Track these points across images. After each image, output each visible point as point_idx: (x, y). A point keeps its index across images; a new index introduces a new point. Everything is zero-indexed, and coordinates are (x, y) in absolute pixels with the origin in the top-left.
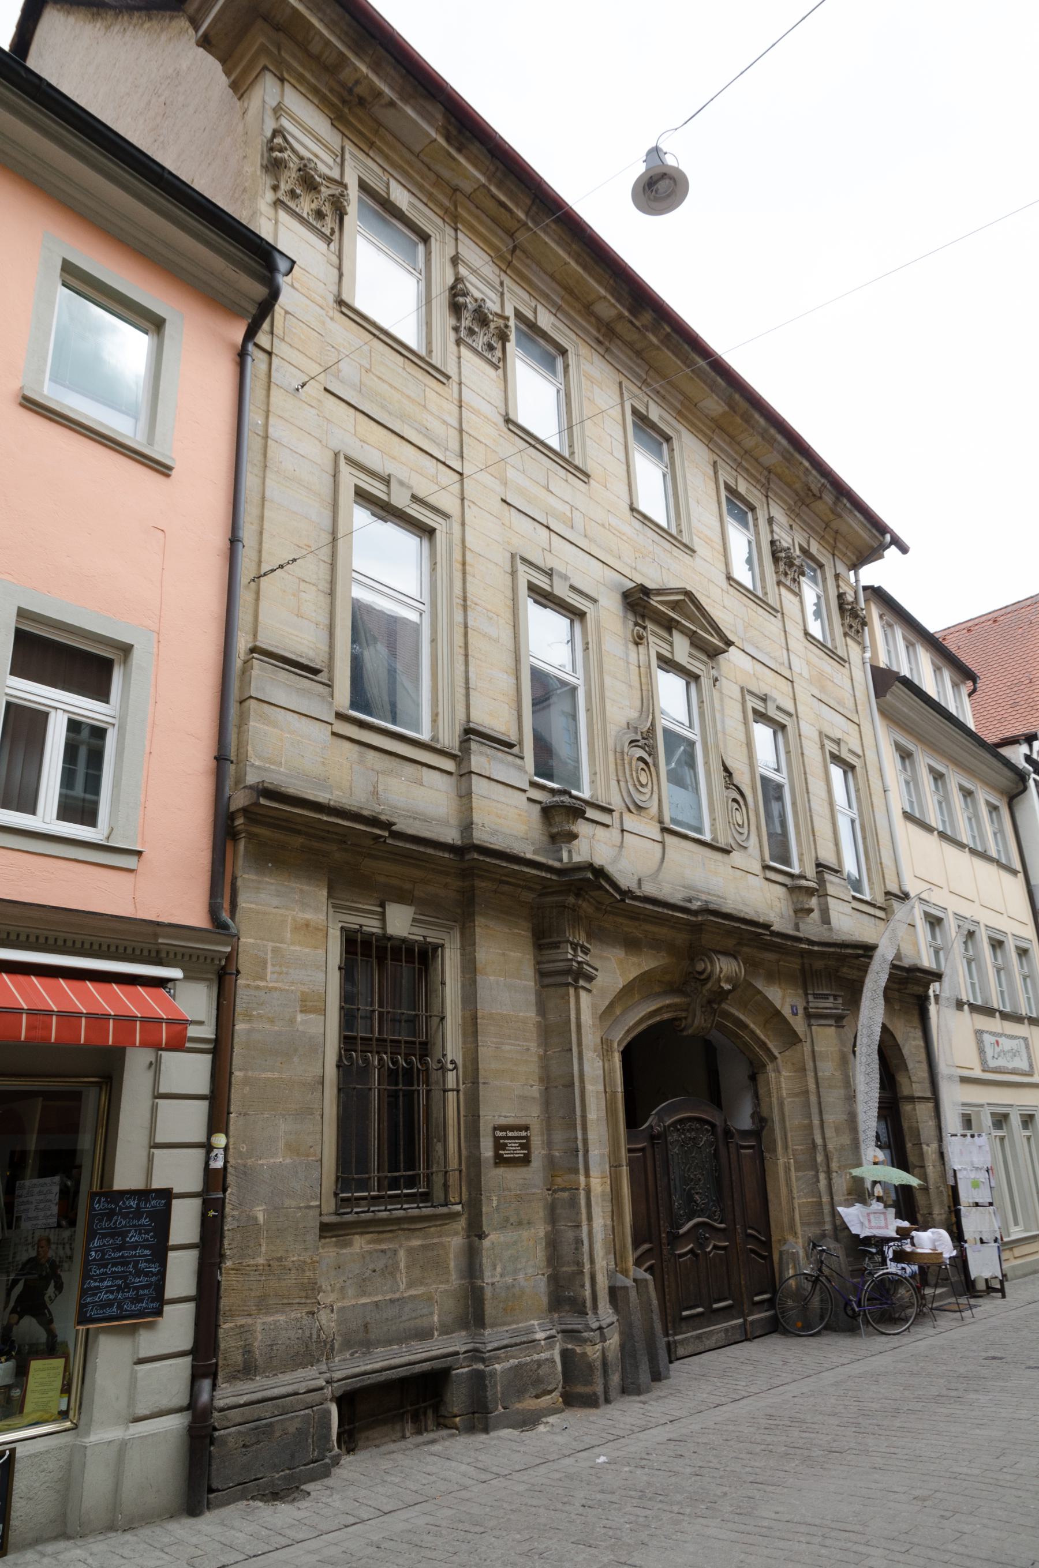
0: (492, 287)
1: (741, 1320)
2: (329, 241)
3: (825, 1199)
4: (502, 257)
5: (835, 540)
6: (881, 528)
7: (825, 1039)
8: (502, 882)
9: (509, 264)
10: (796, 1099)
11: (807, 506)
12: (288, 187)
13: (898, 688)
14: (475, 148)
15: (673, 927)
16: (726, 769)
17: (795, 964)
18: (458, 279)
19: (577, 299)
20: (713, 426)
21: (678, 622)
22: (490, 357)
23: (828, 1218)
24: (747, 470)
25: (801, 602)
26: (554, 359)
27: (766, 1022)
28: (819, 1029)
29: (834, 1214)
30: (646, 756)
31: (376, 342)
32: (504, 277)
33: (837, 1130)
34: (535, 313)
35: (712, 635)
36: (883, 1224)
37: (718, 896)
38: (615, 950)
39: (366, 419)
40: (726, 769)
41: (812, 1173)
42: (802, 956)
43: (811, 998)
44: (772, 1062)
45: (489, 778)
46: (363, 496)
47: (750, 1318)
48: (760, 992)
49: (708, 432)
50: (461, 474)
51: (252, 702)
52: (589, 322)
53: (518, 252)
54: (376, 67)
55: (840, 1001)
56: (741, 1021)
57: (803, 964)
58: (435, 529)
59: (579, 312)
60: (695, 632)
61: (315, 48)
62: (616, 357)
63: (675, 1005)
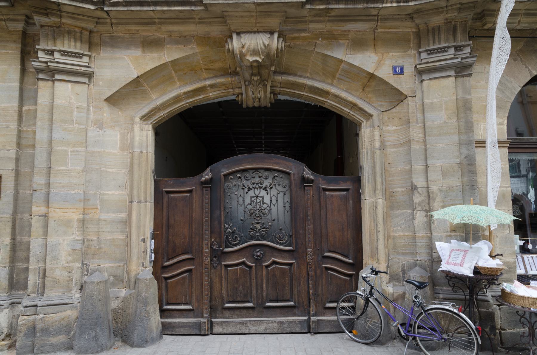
1: (306, 318)
3: (421, 233)
7: (441, 91)
10: (401, 149)
15: (200, 23)
17: (407, 28)
23: (424, 251)
27: (364, 87)
28: (432, 82)
29: (431, 247)
33: (445, 174)
36: (459, 261)
38: (129, 51)
41: (410, 211)
42: (412, 18)
43: (424, 55)
44: (368, 119)
47: (313, 318)
48: (341, 61)
56: (318, 88)
57: (417, 26)
63: (223, 84)
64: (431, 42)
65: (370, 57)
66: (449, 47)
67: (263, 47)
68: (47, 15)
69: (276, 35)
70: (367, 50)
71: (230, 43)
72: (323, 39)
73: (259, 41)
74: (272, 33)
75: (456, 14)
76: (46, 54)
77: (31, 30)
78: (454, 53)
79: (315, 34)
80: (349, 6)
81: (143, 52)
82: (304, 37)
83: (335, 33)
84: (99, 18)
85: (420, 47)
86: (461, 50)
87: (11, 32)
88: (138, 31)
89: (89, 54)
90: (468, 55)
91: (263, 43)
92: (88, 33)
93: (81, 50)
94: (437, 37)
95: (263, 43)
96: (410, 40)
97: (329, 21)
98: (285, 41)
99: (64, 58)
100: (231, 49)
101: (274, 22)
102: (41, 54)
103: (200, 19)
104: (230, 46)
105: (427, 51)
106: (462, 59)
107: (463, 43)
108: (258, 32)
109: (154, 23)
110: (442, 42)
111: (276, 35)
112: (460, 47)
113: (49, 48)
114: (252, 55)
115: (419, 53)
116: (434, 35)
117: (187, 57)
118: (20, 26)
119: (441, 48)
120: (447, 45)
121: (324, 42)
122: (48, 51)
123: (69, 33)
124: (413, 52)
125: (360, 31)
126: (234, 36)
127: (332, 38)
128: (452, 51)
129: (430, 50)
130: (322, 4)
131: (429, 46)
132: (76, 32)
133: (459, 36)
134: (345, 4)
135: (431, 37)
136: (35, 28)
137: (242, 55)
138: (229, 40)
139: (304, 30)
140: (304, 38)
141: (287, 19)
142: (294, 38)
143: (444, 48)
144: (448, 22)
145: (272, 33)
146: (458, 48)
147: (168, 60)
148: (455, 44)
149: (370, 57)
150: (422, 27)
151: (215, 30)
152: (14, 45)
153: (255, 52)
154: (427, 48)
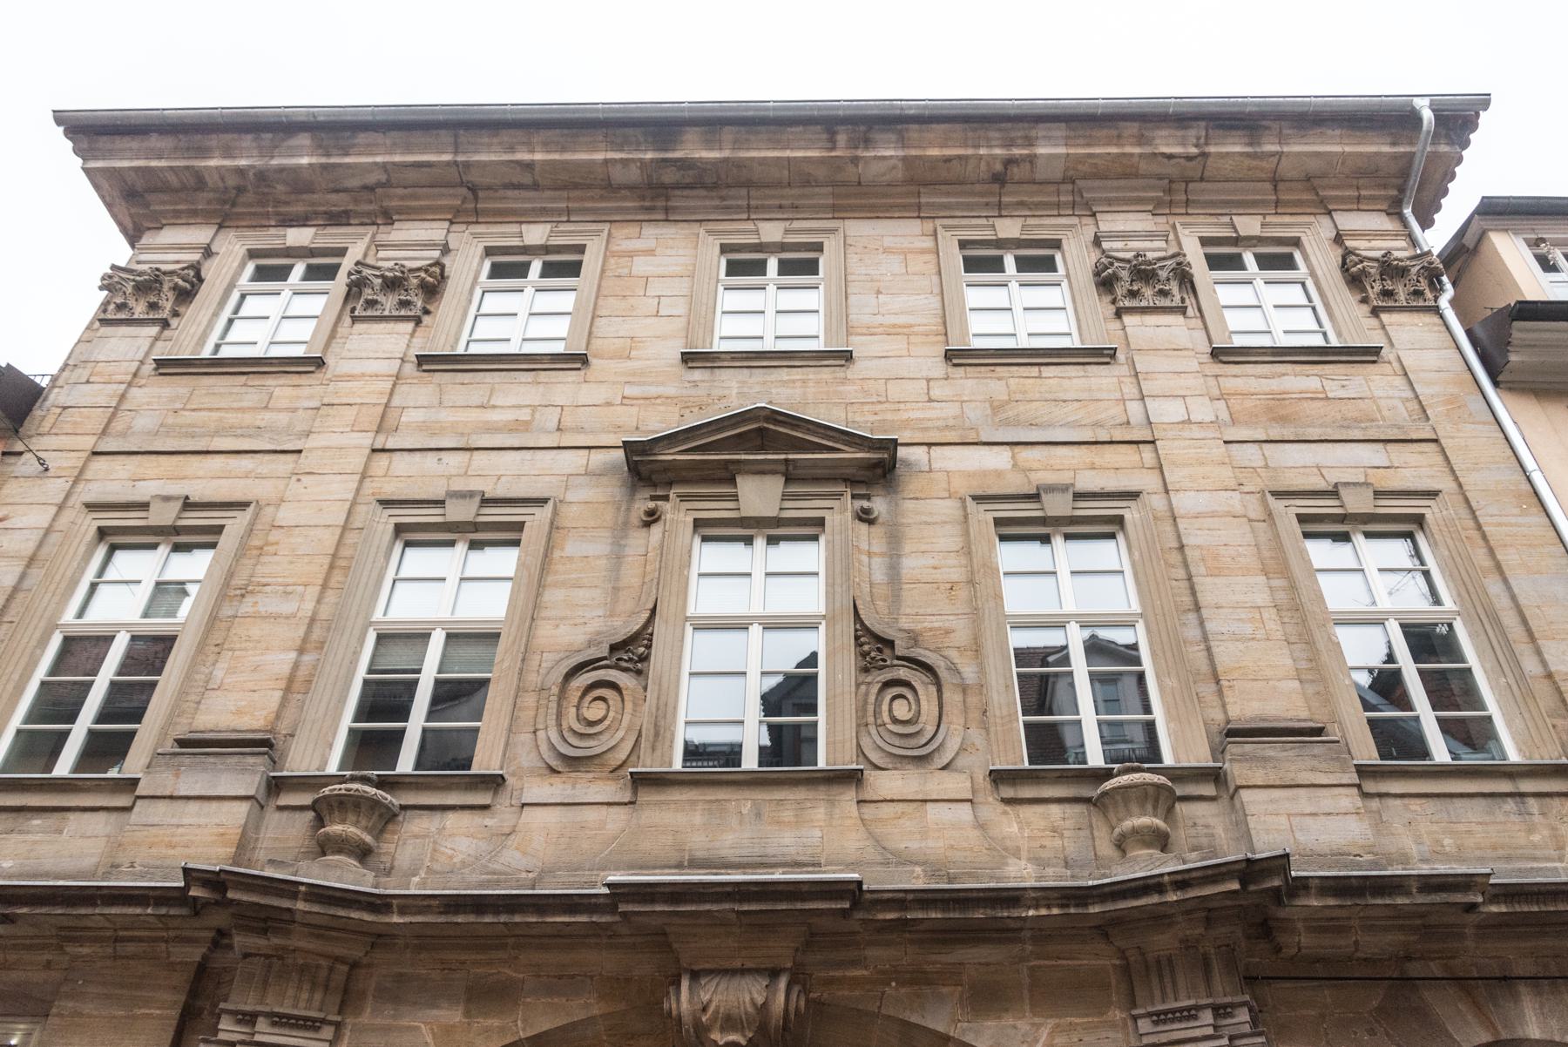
0: (1396, 235)
2: (1182, 310)
4: (1159, 203)
5: (1314, 189)
6: (1393, 119)
8: (117, 940)
9: (477, 212)
11: (1202, 179)
12: (1378, 287)
13: (1521, 331)
14: (362, 138)
16: (653, 611)
18: (1348, 252)
19: (589, 187)
20: (913, 188)
21: (738, 461)
22: (1421, 303)
24: (1022, 204)
25: (1441, 317)
26: (1290, 257)
30: (887, 675)
31: (998, 369)
32: (1172, 219)
34: (1234, 227)
35: (838, 450)
37: (797, 865)
39: (153, 457)
40: (653, 611)
42: (1106, 936)
43: (1145, 1025)
45: (171, 797)
46: (1312, 526)
49: (260, 210)
50: (1436, 441)
51: (1244, 794)
52: (624, 199)
53: (481, 194)
54: (228, 153)
55: (1243, 1016)
58: (1423, 515)
59: (602, 198)
60: (786, 460)
61: (173, 180)
62: (688, 210)
64: (1157, 993)
65: (1015, 1027)
66: (1198, 1008)
67: (750, 1009)
68: (264, 932)
69: (782, 983)
70: (1007, 1010)
71: (673, 998)
72: (901, 984)
73: (746, 994)
74: (774, 974)
75: (1200, 930)
76: (239, 1022)
77: (221, 960)
78: (1211, 1021)
79: (883, 972)
80: (951, 915)
81: (467, 1014)
82: (854, 978)
83: (929, 968)
84: (380, 936)
85: (1134, 1005)
86: (1231, 1015)
87: (171, 966)
88: (463, 963)
89: (339, 1018)
90: (1247, 1029)
91: (752, 999)
92: (345, 968)
93: (321, 1010)
94: (1169, 986)
95: (752, 999)
96: (1109, 984)
97: (912, 942)
98: (805, 990)
99: (276, 1030)
100: (674, 1013)
101: (781, 949)
102: (225, 1024)
103: (610, 937)
104: (674, 1006)
105: (1150, 1015)
106: (1231, 1038)
107: (1228, 1000)
108: (743, 972)
109: (504, 947)
110: (1182, 993)
111: (782, 983)
112: (1225, 1006)
113: (248, 1008)
114: (723, 1030)
115: (1135, 1018)
116: (1161, 976)
117: (574, 1025)
118: (195, 954)
119: (1181, 1010)
120: (1192, 1002)
121: (903, 991)
122: (244, 1014)
123: (303, 970)
124: (1117, 1015)
125: (988, 964)
126: (685, 984)
127: (919, 980)
128: (1207, 1017)
129: (1158, 1014)
130: (890, 911)
131: (1153, 1004)
132: (318, 967)
133: (1218, 985)
134: (943, 911)
135: (1155, 981)
136: (231, 955)
137: (701, 1030)
138: (671, 989)
139: (854, 963)
140: (855, 982)
141: (813, 940)
142: (830, 982)
143: (1189, 1009)
144: (1188, 945)
145: (774, 974)
146: (1220, 1011)
147: (522, 1035)
148: (1210, 1001)
149: (1015, 1027)
150: (1133, 956)
151: (644, 966)
152: (167, 996)
153: (729, 1023)
154: (1150, 1009)
